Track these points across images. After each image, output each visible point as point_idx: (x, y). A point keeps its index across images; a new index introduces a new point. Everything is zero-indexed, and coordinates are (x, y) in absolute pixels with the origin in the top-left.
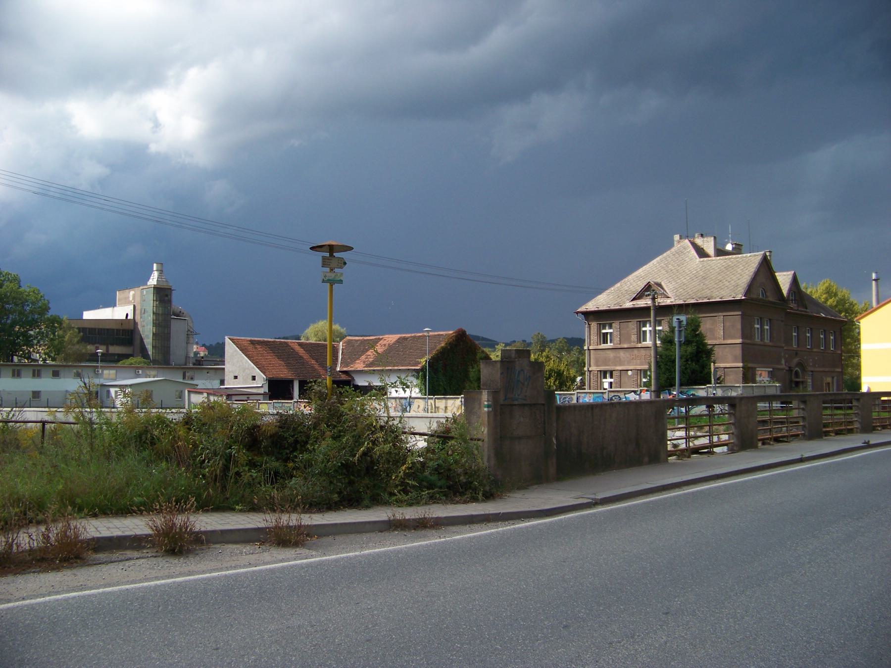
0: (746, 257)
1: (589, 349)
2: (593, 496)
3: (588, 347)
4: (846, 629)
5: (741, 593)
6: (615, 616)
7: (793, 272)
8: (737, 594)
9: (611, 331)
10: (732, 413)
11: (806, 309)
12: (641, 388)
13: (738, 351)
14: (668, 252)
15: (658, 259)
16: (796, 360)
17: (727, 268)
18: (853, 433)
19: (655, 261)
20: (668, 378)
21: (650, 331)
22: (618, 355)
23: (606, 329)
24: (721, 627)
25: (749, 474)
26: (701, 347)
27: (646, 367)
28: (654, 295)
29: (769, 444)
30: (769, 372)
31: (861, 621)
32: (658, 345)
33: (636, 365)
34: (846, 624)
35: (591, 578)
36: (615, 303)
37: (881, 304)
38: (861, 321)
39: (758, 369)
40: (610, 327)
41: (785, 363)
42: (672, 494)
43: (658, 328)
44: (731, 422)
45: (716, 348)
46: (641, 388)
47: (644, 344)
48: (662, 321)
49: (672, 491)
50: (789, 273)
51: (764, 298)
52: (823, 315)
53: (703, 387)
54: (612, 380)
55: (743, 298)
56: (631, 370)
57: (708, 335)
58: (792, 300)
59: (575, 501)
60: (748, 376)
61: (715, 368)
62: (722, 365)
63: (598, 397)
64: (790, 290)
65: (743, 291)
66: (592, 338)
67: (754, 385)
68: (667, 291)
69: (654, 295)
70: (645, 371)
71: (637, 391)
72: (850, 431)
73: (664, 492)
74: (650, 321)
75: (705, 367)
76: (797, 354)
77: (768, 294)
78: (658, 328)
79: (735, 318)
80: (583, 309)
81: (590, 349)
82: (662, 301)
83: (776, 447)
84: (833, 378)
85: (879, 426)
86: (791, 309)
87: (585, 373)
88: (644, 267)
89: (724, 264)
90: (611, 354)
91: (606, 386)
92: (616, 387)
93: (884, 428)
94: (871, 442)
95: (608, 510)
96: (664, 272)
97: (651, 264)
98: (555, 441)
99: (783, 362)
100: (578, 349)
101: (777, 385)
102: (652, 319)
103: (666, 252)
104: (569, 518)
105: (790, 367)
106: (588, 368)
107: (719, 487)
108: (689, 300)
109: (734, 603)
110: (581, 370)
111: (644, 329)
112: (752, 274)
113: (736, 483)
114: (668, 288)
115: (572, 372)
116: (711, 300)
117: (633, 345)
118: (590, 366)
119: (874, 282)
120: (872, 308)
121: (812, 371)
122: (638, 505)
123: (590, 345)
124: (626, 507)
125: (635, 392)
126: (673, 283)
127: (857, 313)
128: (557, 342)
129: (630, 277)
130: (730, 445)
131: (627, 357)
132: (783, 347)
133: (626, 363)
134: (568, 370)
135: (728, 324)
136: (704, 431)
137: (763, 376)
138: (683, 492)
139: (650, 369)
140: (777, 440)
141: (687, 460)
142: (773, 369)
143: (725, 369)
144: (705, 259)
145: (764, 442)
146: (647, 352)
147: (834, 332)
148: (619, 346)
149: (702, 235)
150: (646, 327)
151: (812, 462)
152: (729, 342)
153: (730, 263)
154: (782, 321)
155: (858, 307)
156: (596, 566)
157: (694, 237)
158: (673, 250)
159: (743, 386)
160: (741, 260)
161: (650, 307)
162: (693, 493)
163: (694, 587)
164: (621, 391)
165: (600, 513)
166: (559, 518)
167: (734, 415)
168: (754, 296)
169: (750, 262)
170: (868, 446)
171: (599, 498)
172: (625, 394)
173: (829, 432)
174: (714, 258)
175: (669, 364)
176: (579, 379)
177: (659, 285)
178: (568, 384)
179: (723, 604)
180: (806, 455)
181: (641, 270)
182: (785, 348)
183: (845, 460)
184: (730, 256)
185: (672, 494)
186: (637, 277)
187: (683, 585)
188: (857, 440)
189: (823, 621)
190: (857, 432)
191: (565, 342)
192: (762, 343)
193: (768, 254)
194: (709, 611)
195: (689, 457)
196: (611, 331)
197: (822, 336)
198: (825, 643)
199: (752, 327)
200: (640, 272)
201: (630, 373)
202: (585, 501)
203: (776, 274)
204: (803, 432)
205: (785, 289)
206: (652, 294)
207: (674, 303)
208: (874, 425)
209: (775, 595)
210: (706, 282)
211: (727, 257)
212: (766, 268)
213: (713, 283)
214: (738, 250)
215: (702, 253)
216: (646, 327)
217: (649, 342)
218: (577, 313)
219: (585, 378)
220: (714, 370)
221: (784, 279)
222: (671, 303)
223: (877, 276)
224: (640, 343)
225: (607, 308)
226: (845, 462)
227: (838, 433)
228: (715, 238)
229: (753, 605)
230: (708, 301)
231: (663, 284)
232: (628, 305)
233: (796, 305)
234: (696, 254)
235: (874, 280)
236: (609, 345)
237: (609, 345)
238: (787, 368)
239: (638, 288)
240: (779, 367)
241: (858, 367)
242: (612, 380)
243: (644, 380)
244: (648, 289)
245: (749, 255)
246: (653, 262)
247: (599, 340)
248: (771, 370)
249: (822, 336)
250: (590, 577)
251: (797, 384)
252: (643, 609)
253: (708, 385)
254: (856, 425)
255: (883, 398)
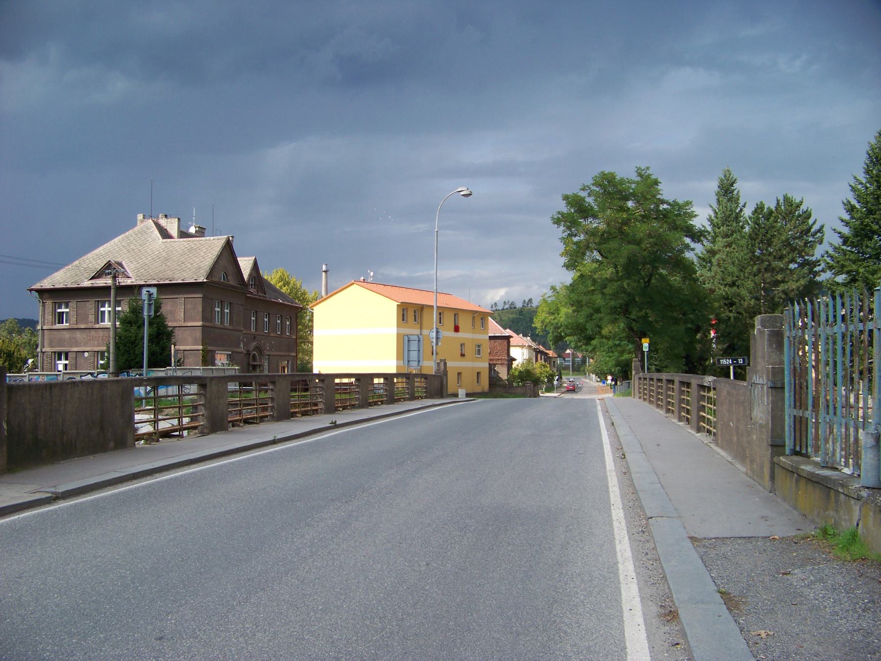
0: (209, 240)
1: (42, 329)
2: (53, 490)
3: (42, 327)
4: (373, 636)
5: (245, 601)
6: (94, 650)
7: (254, 258)
8: (240, 603)
9: (67, 310)
10: (202, 394)
11: (265, 294)
12: (98, 370)
13: (199, 334)
14: (131, 232)
15: (120, 237)
16: (254, 344)
17: (190, 250)
18: (317, 413)
19: (116, 240)
20: (127, 360)
21: (109, 312)
22: (74, 336)
23: (61, 308)
24: (231, 651)
25: (224, 458)
26: (162, 328)
27: (104, 348)
28: (115, 274)
29: (239, 426)
30: (227, 355)
31: (385, 622)
32: (117, 326)
33: (94, 346)
34: (371, 628)
35: (58, 597)
36: (73, 281)
37: (329, 295)
38: (314, 308)
39: (217, 352)
40: (67, 307)
41: (244, 347)
42: (144, 483)
43: (119, 309)
44: (201, 403)
45: (177, 331)
46: (98, 370)
47: (102, 325)
48: (122, 302)
49: (144, 479)
50: (250, 258)
51: (226, 282)
52: (281, 301)
53: (163, 369)
54: (67, 362)
55: (205, 280)
56: (87, 352)
57: (169, 317)
58: (252, 285)
59: (31, 496)
60: (208, 359)
61: (176, 351)
62: (182, 348)
63: (52, 379)
64: (250, 275)
65: (205, 274)
66: (46, 318)
67: (214, 367)
68: (128, 271)
69: (115, 274)
70: (103, 353)
71: (94, 373)
72: (315, 412)
73: (135, 481)
74: (109, 302)
75: (165, 349)
76: (255, 338)
77: (229, 278)
78: (119, 309)
79: (196, 300)
80: (37, 286)
81: (44, 328)
82: (124, 281)
83: (247, 429)
84: (288, 362)
85: (341, 407)
86: (251, 293)
87: (37, 356)
88: (105, 245)
89: (187, 246)
90: (67, 335)
91: (61, 367)
92: (71, 369)
93: (343, 409)
94: (338, 423)
95: (71, 506)
96: (125, 251)
97: (112, 242)
98: (5, 426)
99: (242, 345)
100: (29, 330)
101: (236, 368)
102: (112, 299)
103: (128, 230)
104: (24, 519)
105: (248, 351)
106: (41, 350)
107: (195, 473)
108: (150, 281)
109: (239, 615)
110: (33, 352)
111: (102, 309)
112: (214, 257)
113: (211, 468)
114: (129, 268)
115: (24, 352)
116: (172, 282)
117: (90, 325)
118: (43, 346)
119: (324, 273)
120: (322, 297)
121: (269, 355)
122: (106, 497)
123: (44, 325)
124: (92, 501)
125: (92, 374)
126: (135, 263)
127: (308, 301)
128: (7, 322)
129: (90, 255)
130: (199, 428)
131: (84, 338)
132: (242, 331)
133: (82, 344)
134: (19, 350)
135: (189, 306)
136: (163, 414)
137: (221, 359)
138: (156, 480)
139: (108, 352)
140: (247, 422)
141: (155, 445)
142: (232, 352)
143: (185, 352)
144: (168, 240)
145: (234, 424)
146: (106, 333)
147: (290, 318)
148: (75, 327)
149: (166, 216)
150: (105, 307)
151: (284, 443)
152: (190, 324)
153: (193, 246)
154: (242, 305)
155: (310, 296)
156: (63, 580)
157: (158, 217)
158: (136, 229)
159: (203, 369)
160: (204, 243)
161: (110, 286)
162: (167, 480)
163: (187, 598)
164: (77, 373)
165: (62, 509)
166: (12, 518)
167: (204, 395)
168: (216, 279)
169: (213, 245)
170: (335, 426)
171: (60, 491)
172: (81, 376)
173: (296, 413)
174: (177, 240)
175: (128, 345)
176: (30, 361)
177: (120, 264)
178: (19, 366)
179: (227, 617)
180: (279, 436)
181: (101, 248)
182: (244, 332)
183: (317, 440)
184: (194, 239)
185: (144, 483)
186: (97, 255)
187: (174, 597)
188: (324, 420)
189: (345, 627)
190: (321, 413)
191: (16, 323)
192: (222, 326)
193: (231, 238)
194: (212, 630)
195: (158, 441)
196: (67, 310)
197: (279, 321)
198: (355, 657)
199: (213, 309)
200: (100, 250)
201: (86, 354)
202: (44, 496)
203: (238, 259)
204: (271, 413)
205: (246, 273)
206: (113, 272)
207: (135, 284)
208: (336, 405)
209: (284, 600)
210: (169, 263)
211: (190, 239)
212: (228, 251)
213: (176, 265)
214: (201, 232)
215: (165, 234)
216: (105, 307)
217: (107, 323)
218: (31, 290)
219: (37, 362)
220: (175, 352)
221: (245, 265)
222: (131, 284)
223: (327, 267)
224: (98, 323)
225: (64, 286)
226: (317, 442)
227: (305, 414)
228: (179, 219)
229: (262, 616)
230: (170, 282)
231: (123, 263)
232: (87, 284)
233: (255, 290)
234: (159, 235)
235: (324, 271)
236: (65, 325)
237: (65, 325)
238: (245, 352)
239: (97, 267)
240: (238, 350)
241: (310, 353)
242: (67, 362)
243: (102, 362)
244: (109, 268)
245: (212, 238)
246: (114, 240)
247: (54, 319)
248: (230, 353)
249: (279, 321)
250: (56, 595)
251: (254, 367)
252: (129, 636)
253: (167, 368)
254: (321, 406)
255: (337, 381)
